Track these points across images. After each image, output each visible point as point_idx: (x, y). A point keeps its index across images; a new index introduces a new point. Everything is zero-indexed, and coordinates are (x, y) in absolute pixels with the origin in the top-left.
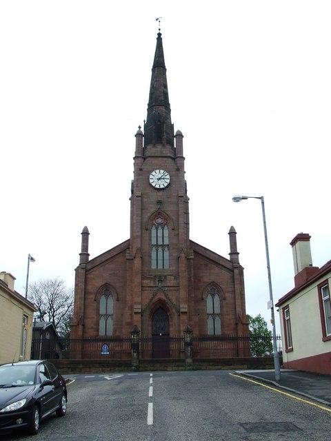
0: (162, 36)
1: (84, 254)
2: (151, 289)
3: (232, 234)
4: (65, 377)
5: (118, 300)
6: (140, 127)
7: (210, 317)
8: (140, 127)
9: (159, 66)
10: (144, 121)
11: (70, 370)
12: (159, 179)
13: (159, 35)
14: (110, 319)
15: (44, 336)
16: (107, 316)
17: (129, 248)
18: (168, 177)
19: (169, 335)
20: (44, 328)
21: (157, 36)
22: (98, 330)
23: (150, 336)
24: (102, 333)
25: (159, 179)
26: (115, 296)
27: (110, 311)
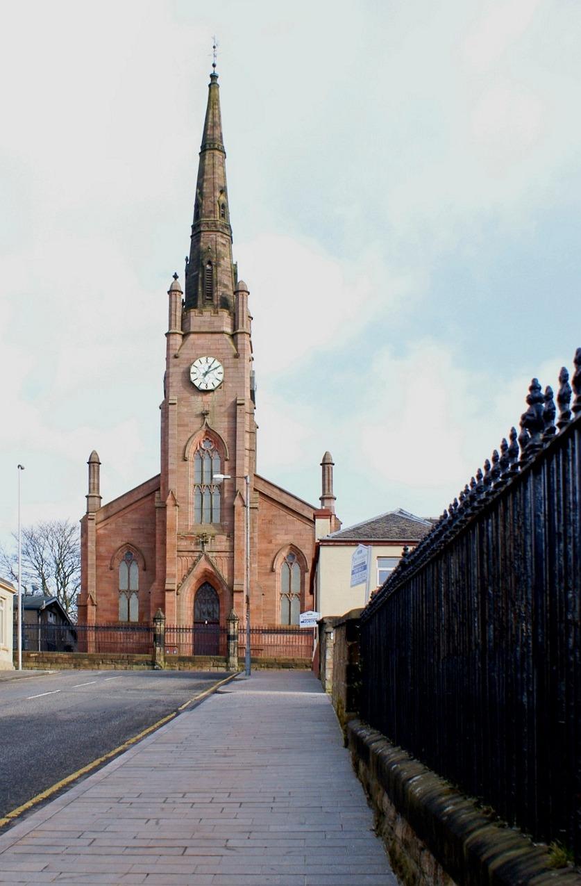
0: (218, 81)
1: (93, 494)
2: (191, 554)
3: (326, 464)
4: (408, 547)
5: (145, 570)
6: (176, 277)
7: (123, 597)
8: (176, 277)
9: (211, 145)
10: (187, 259)
11: (73, 666)
12: (205, 375)
13: (213, 77)
14: (134, 596)
15: (45, 618)
16: (129, 592)
17: (158, 489)
18: (217, 364)
19: (218, 623)
20: (44, 607)
21: (209, 81)
22: (117, 613)
23: (190, 624)
24: (122, 618)
25: (205, 375)
26: (141, 565)
27: (135, 585)
